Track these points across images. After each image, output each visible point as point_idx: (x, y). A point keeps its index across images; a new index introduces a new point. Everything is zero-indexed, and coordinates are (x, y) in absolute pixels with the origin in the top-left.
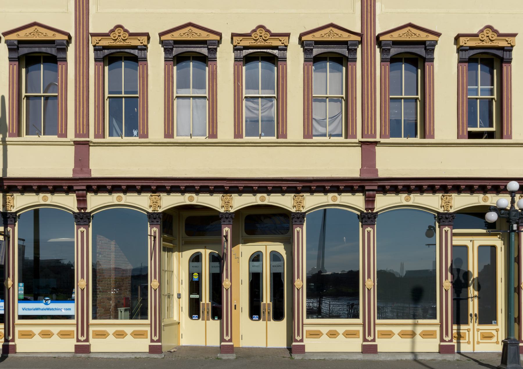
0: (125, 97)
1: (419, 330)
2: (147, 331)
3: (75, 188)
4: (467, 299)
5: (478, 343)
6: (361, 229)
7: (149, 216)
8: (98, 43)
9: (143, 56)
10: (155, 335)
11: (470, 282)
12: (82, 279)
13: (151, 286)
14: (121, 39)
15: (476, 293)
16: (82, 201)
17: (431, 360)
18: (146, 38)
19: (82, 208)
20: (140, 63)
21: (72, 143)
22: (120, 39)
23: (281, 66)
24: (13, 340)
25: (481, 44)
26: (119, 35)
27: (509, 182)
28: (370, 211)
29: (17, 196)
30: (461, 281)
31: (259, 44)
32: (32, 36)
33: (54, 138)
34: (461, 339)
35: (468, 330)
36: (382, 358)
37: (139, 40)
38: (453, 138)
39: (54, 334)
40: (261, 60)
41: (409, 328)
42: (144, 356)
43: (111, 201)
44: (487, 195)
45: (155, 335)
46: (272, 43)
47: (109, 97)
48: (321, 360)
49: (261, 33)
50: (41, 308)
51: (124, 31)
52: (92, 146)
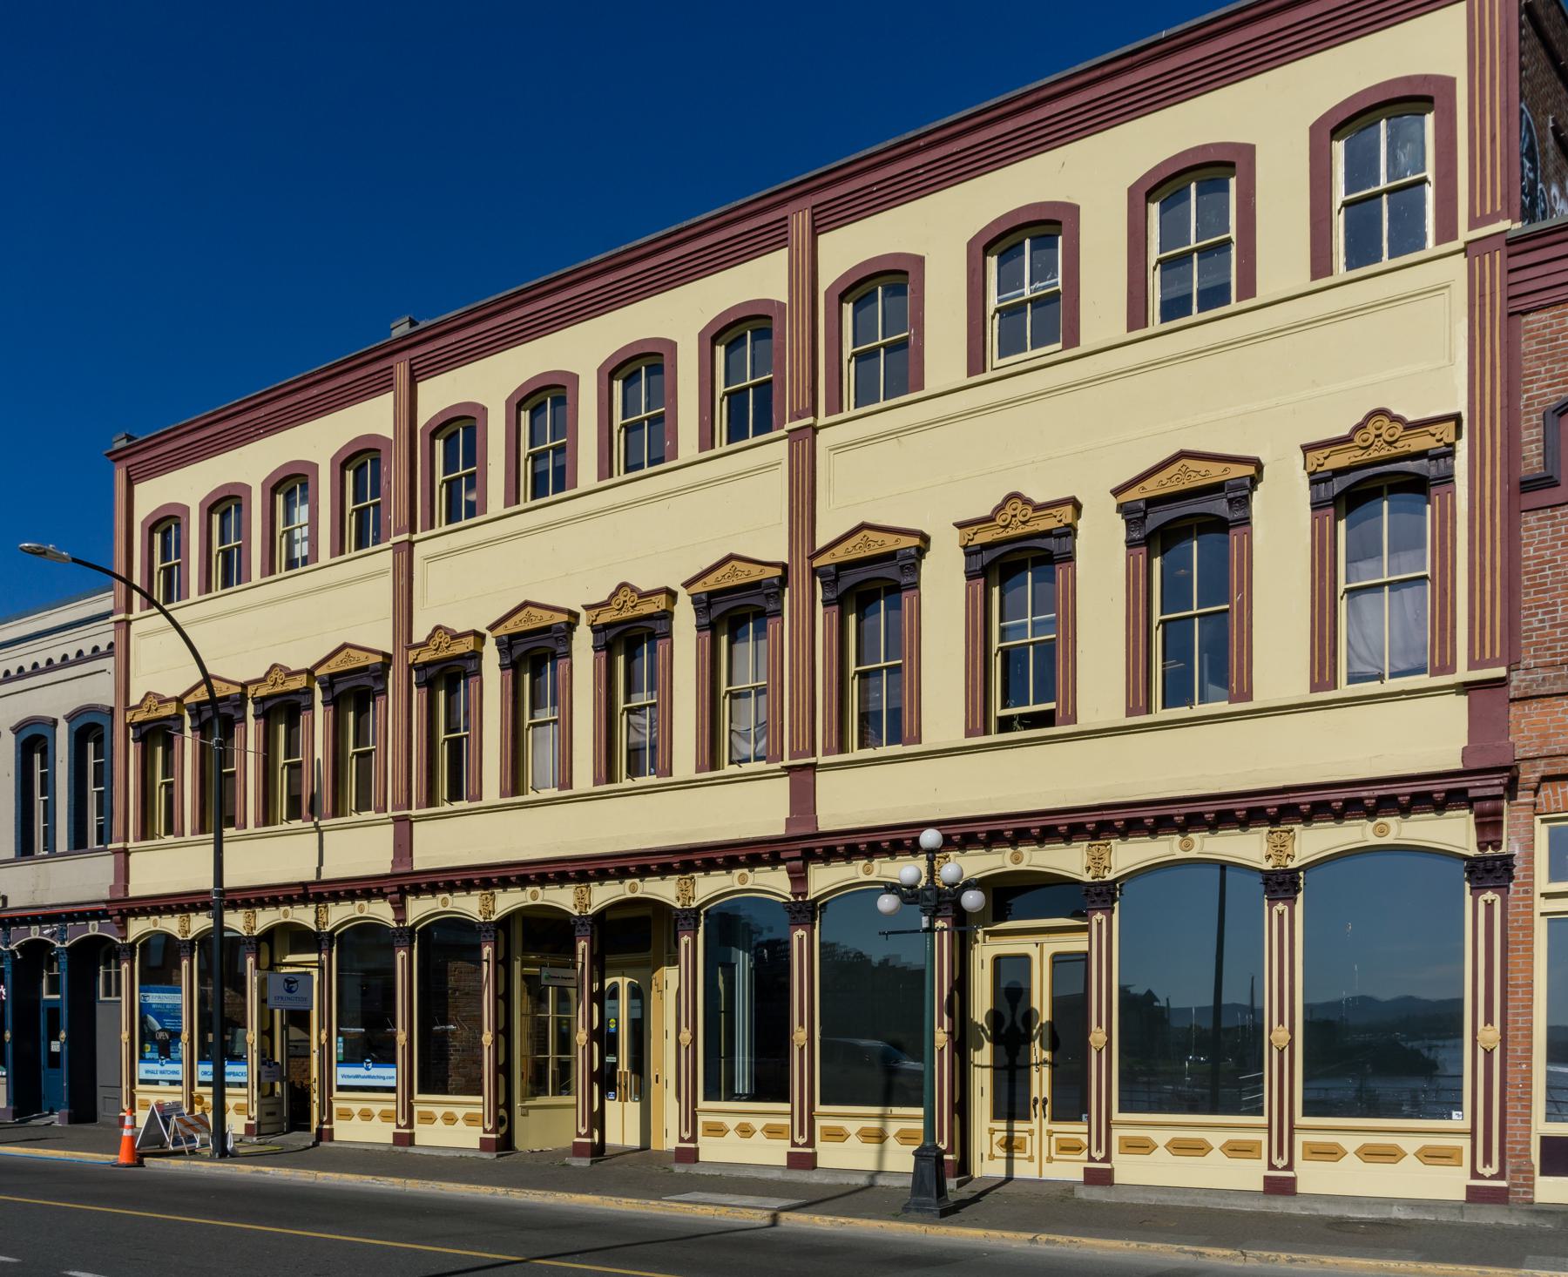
0: (1199, 616)
1: (893, 1127)
3: (783, 856)
4: (1028, 1066)
5: (1050, 1159)
6: (1469, 899)
8: (1322, 465)
11: (1035, 1031)
13: (1270, 1041)
14: (1382, 442)
15: (1047, 1055)
16: (799, 879)
17: (900, 1188)
19: (799, 894)
20: (1232, 532)
21: (391, 820)
22: (1379, 444)
23: (1437, 497)
24: (330, 1121)
25: (1004, 535)
26: (1378, 432)
27: (923, 831)
29: (412, 900)
30: (1018, 1029)
31: (1374, 454)
32: (859, 551)
33: (1223, 707)
34: (1015, 1150)
35: (1031, 1132)
36: (1126, 1198)
37: (1434, 435)
38: (958, 738)
40: (1389, 493)
41: (875, 1124)
42: (471, 1155)
43: (1168, 852)
44: (1020, 849)
46: (1409, 446)
47: (1163, 622)
48: (714, 1175)
49: (1377, 429)
50: (362, 1075)
51: (1023, 504)
52: (416, 821)
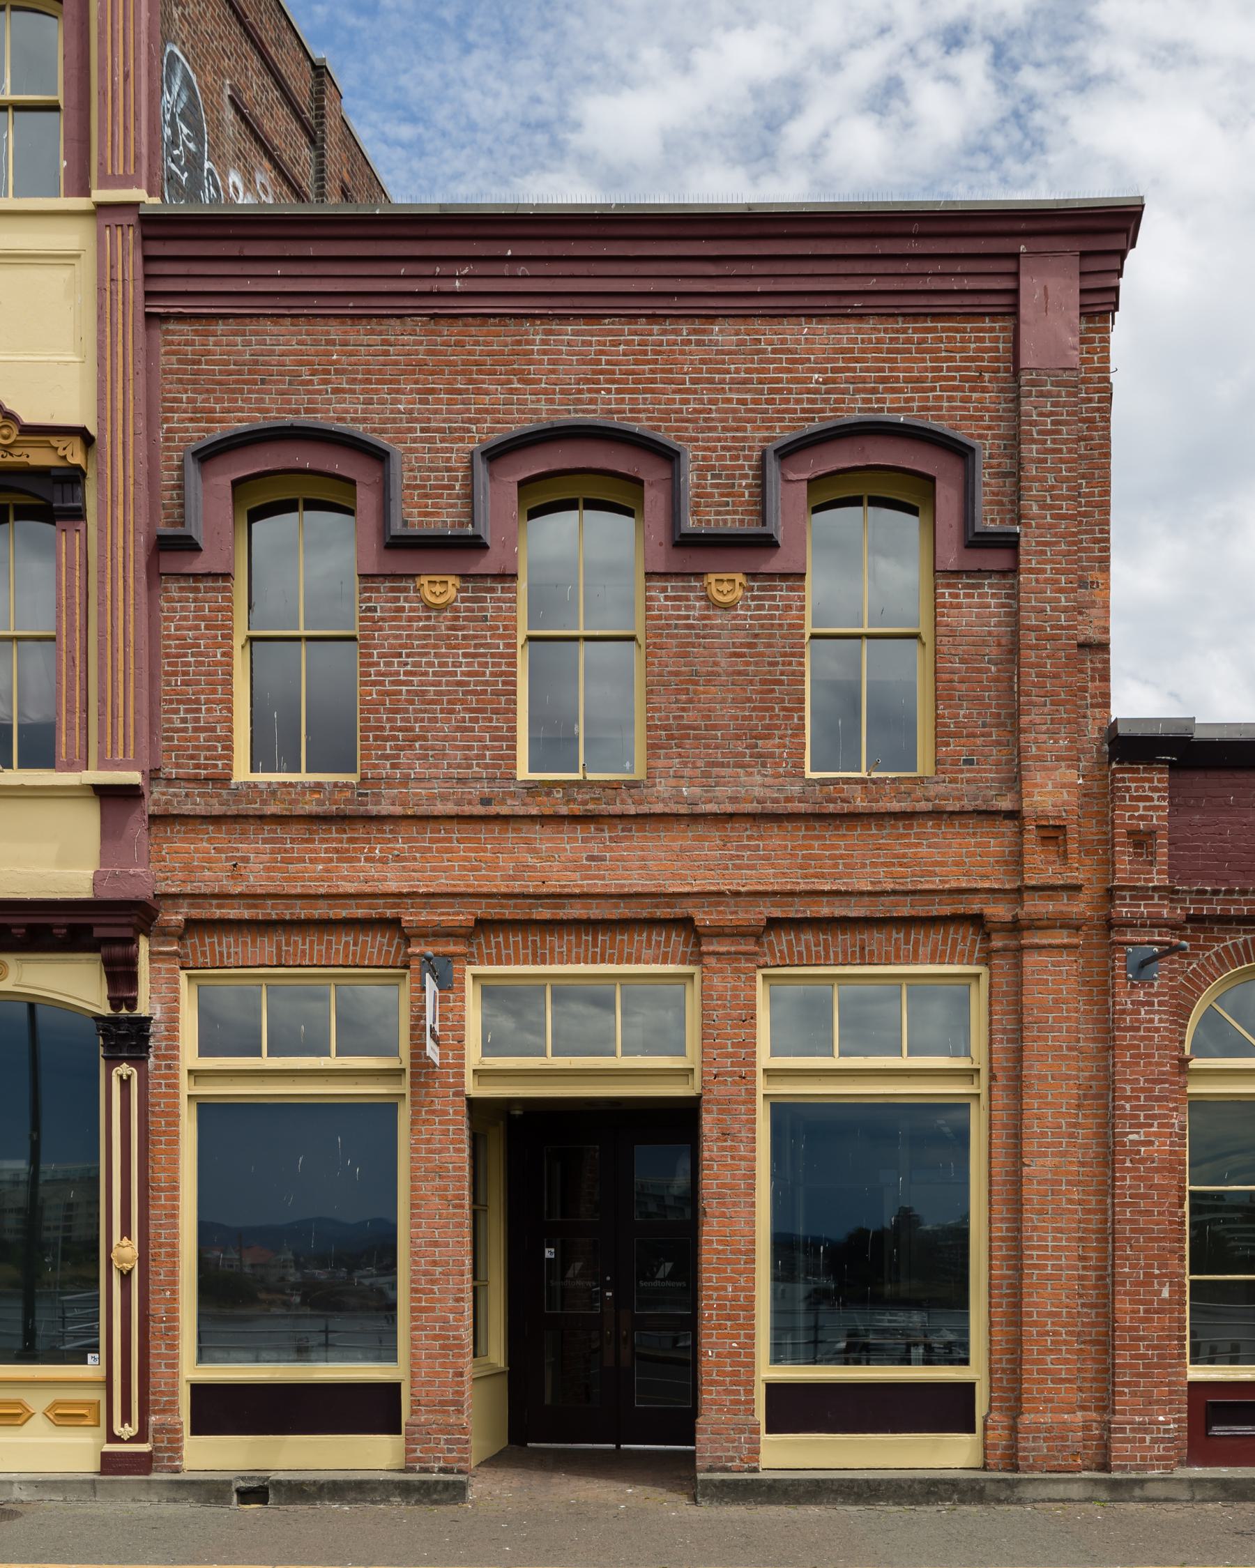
51: (4, 417)
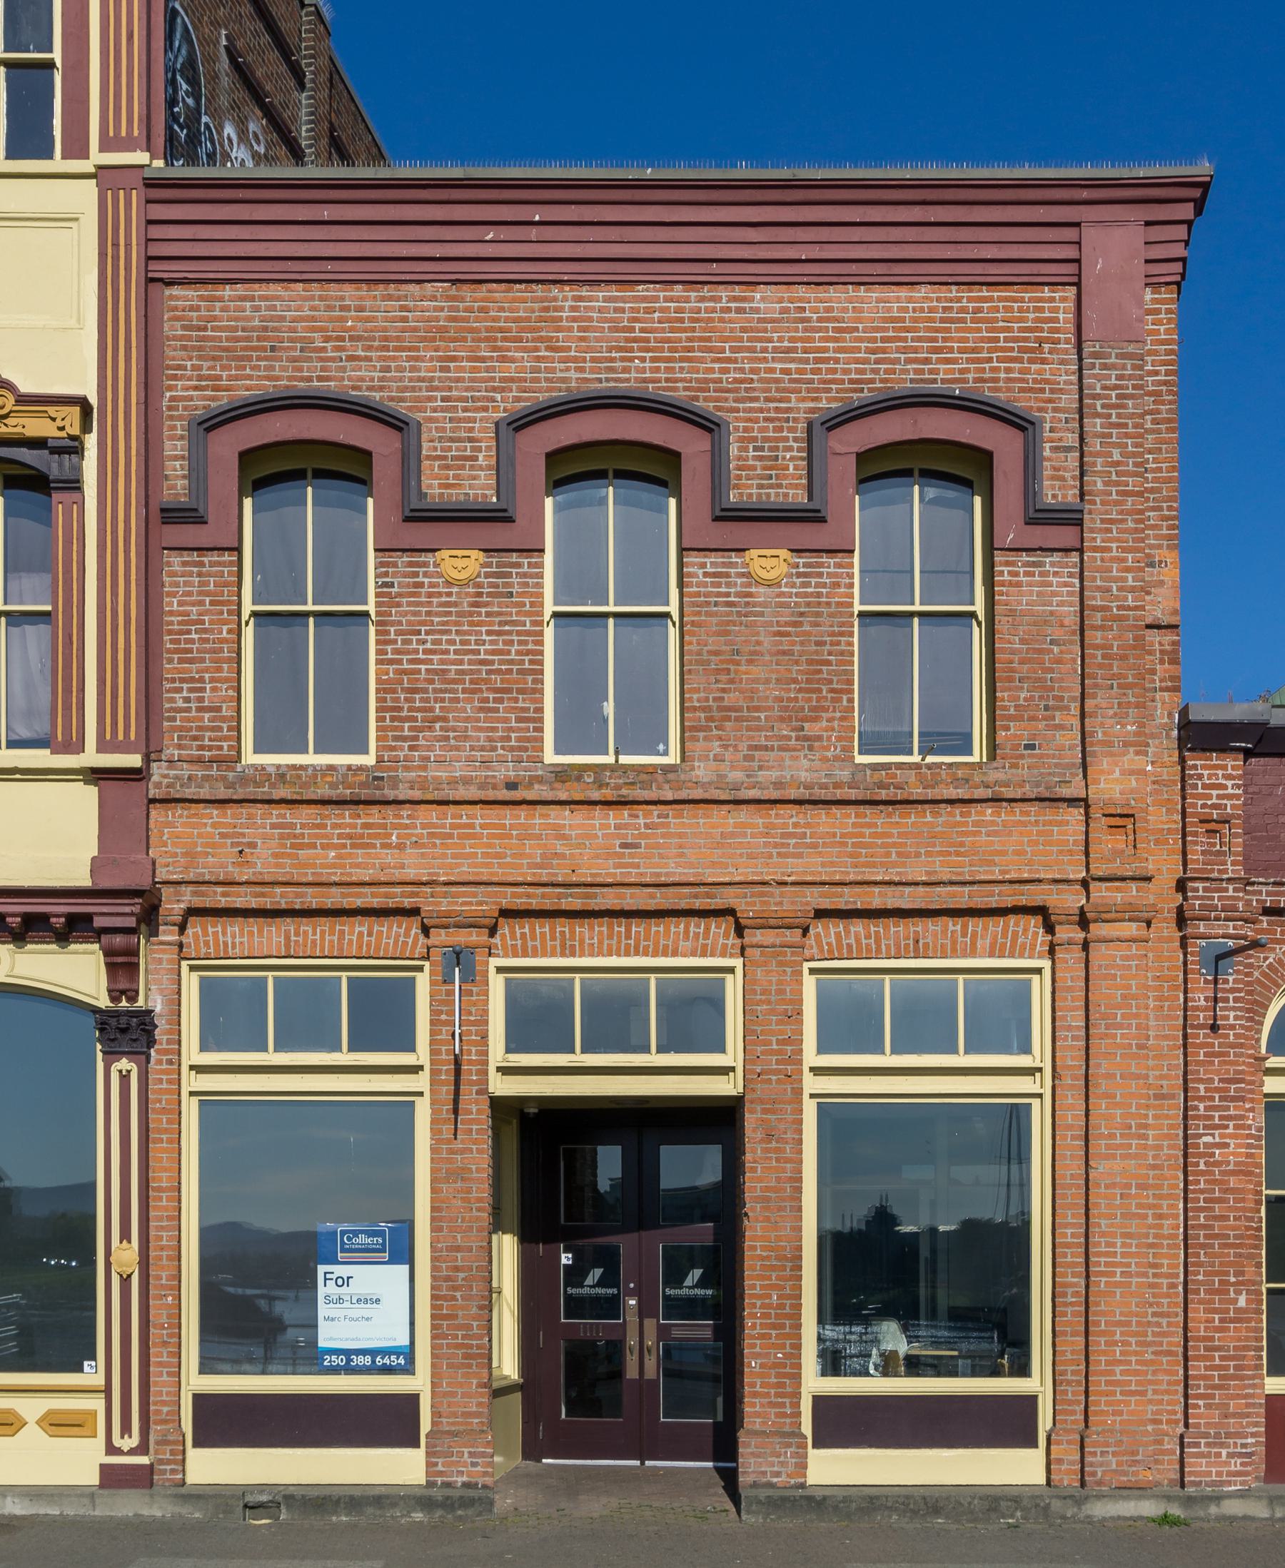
2: (93, 1414)
7: (102, 1024)
9: (67, 474)
10: (126, 1429)
12: (125, 1241)
18: (76, 410)
28: (124, 1003)
30: (703, 1276)
37: (54, 419)
39: (26, 1423)
45: (126, 1429)
